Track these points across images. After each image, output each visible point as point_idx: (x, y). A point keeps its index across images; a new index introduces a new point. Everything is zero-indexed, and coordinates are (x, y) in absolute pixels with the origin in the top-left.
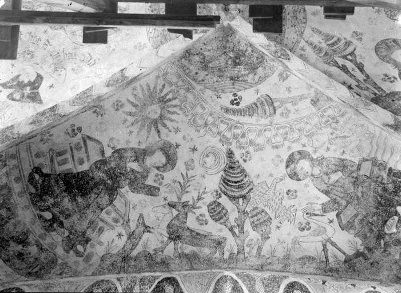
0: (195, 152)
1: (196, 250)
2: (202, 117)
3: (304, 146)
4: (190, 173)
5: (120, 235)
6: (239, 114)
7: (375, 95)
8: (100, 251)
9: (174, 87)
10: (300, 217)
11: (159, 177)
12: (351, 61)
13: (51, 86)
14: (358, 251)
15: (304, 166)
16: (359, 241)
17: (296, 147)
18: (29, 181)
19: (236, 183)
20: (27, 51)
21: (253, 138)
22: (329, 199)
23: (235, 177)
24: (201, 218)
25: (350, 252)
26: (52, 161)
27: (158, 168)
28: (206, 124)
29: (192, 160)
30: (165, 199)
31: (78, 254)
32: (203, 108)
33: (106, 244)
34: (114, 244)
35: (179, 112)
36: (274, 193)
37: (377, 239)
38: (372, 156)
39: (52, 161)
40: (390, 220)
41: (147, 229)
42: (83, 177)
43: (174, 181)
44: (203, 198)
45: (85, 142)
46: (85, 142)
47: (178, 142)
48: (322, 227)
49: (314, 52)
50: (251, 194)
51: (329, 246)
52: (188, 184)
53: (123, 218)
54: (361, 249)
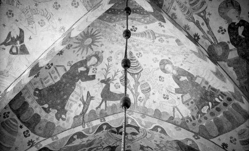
0: (112, 53)
1: (115, 103)
2: (115, 37)
3: (170, 58)
4: (110, 63)
5: (80, 105)
6: (136, 35)
7: (211, 44)
8: (66, 45)
9: (98, 28)
10: (165, 92)
11: (95, 69)
12: (202, 17)
13: (30, 38)
14: (188, 116)
15: (168, 67)
16: (189, 111)
17: (166, 58)
18: (34, 95)
19: (133, 67)
20: (8, 12)
21: (143, 47)
22: (179, 87)
23: (134, 64)
24: (116, 85)
25: (185, 116)
26: (42, 83)
27: (93, 65)
28: (117, 40)
29: (111, 57)
30: (99, 80)
31: (63, 119)
32: (115, 33)
33: (74, 111)
34: (78, 110)
35: (102, 37)
36: (153, 75)
37: (198, 113)
38: (203, 76)
39: (42, 83)
40: (205, 107)
41: (92, 98)
42: (58, 84)
43: (102, 69)
44: (117, 74)
45: (56, 69)
46: (56, 69)
47: (102, 50)
48: (174, 100)
49: (181, 11)
50: (141, 73)
51: (176, 109)
52: (110, 68)
53: (80, 96)
54: (190, 116)
